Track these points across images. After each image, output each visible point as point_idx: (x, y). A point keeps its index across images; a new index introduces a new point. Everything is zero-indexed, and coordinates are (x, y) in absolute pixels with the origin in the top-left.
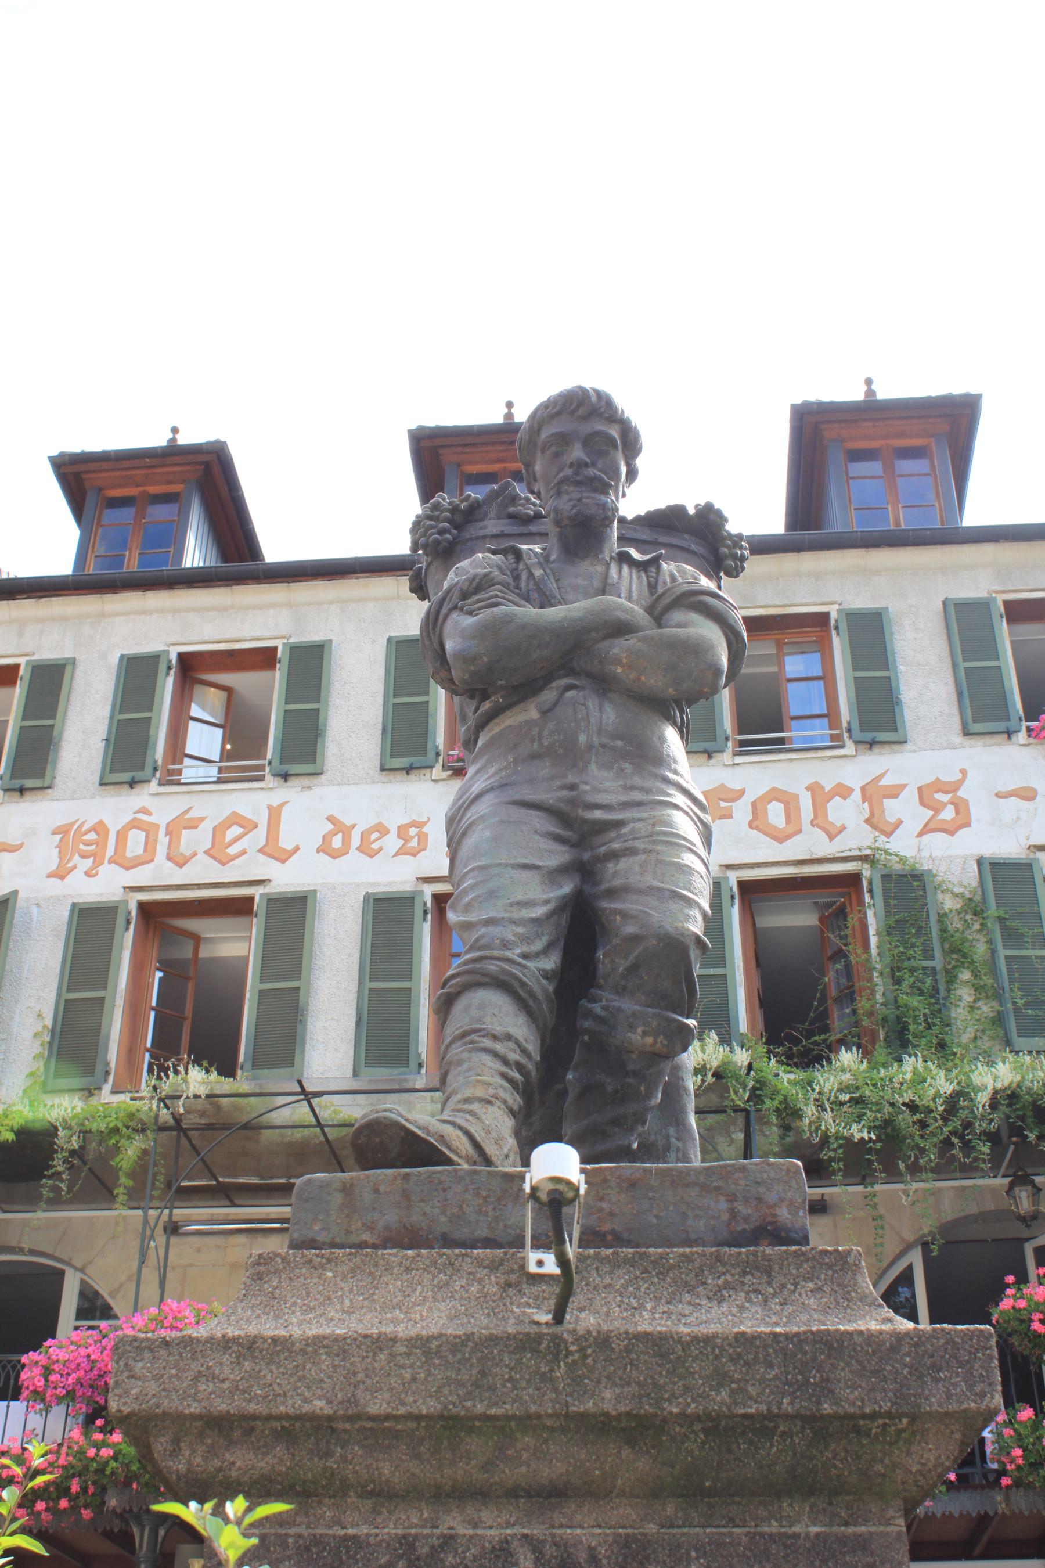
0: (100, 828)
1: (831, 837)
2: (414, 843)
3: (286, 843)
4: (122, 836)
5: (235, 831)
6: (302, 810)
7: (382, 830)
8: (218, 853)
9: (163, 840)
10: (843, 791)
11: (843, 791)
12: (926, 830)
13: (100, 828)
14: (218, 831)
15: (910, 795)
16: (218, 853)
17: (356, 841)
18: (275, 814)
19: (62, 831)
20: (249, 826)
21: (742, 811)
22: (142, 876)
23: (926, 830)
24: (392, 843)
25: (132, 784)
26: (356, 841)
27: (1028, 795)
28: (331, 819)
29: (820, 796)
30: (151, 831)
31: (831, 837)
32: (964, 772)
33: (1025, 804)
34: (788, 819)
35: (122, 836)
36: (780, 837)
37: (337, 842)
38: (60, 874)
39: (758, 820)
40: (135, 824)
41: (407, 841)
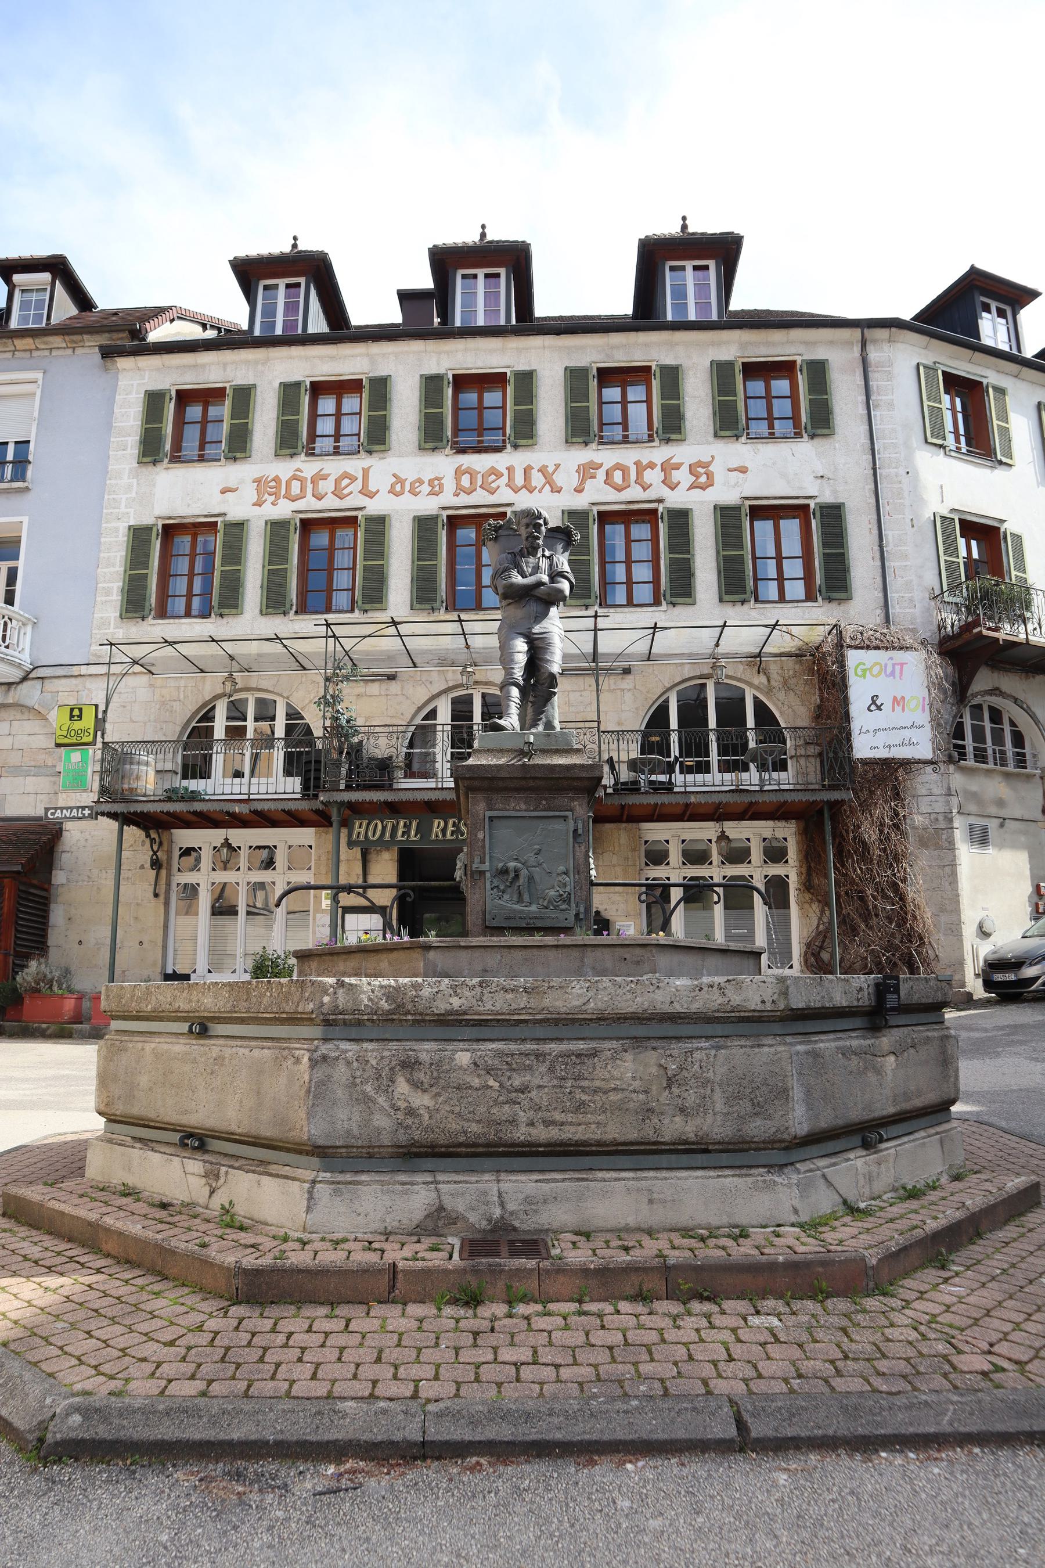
0: (277, 479)
1: (645, 490)
2: (703, 479)
3: (372, 488)
4: (288, 484)
5: (346, 481)
6: (381, 469)
7: (421, 482)
8: (338, 493)
9: (310, 486)
10: (651, 466)
11: (651, 466)
12: (692, 487)
13: (277, 479)
14: (337, 482)
15: (685, 469)
16: (338, 493)
17: (407, 487)
18: (366, 472)
19: (258, 481)
20: (353, 479)
21: (601, 474)
22: (300, 505)
23: (692, 487)
24: (426, 488)
25: (292, 456)
26: (407, 487)
27: (743, 470)
28: (394, 475)
29: (640, 468)
30: (302, 480)
31: (645, 490)
32: (713, 457)
33: (742, 475)
34: (624, 478)
35: (288, 484)
36: (619, 489)
37: (398, 488)
38: (259, 504)
39: (608, 480)
40: (295, 477)
41: (698, 477)
